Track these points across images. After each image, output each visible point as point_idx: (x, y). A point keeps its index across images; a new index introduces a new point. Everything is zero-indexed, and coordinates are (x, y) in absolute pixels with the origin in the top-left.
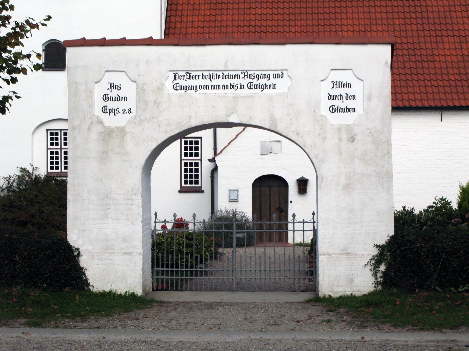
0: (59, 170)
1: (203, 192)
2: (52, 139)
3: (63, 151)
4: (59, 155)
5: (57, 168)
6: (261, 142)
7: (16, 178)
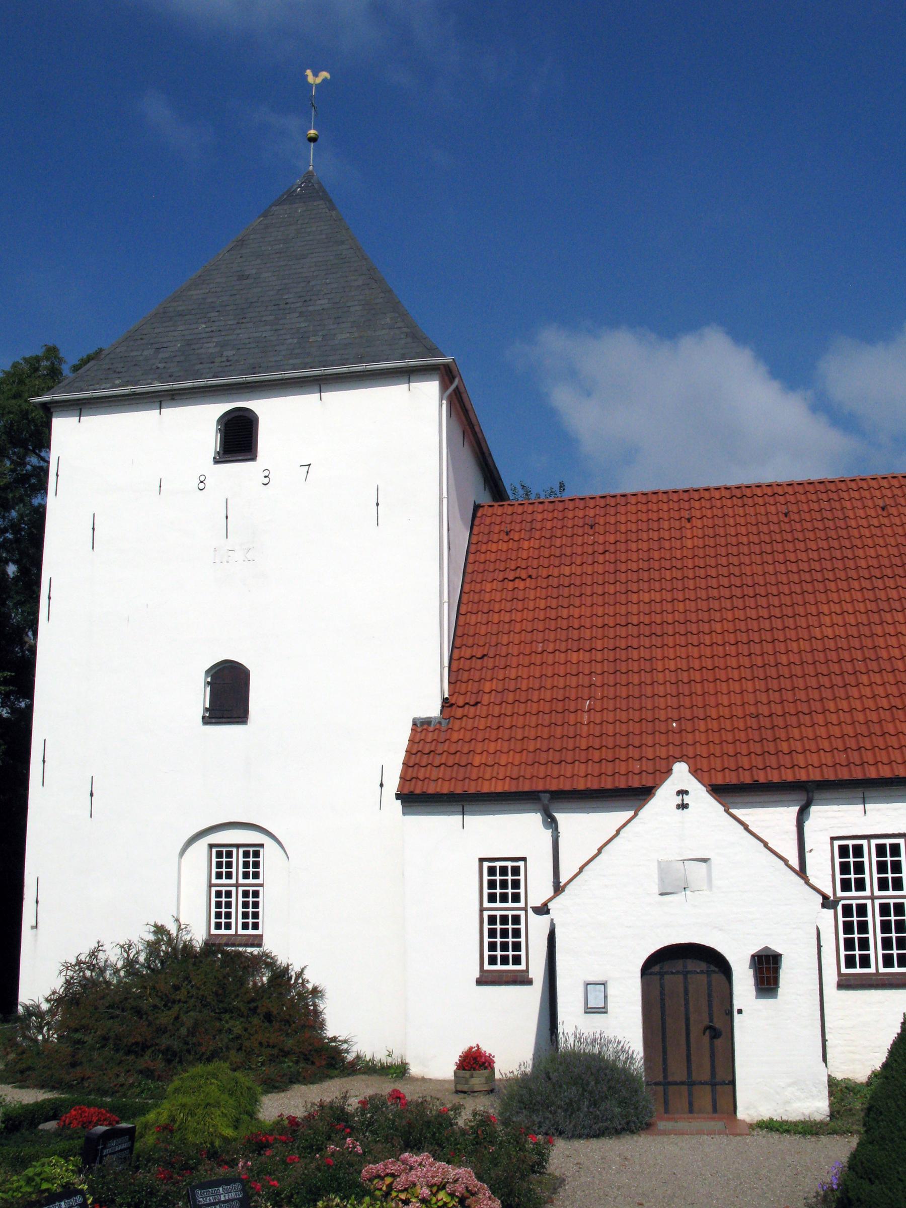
0: (232, 932)
1: (529, 982)
3: (241, 889)
4: (233, 900)
5: (228, 926)
6: (659, 863)
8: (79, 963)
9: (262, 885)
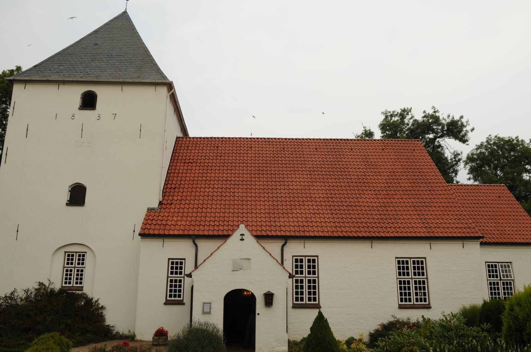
0: (71, 285)
1: (184, 304)
2: (68, 260)
3: (76, 269)
5: (70, 283)
7: (33, 290)
8: (6, 297)
9: (85, 267)
